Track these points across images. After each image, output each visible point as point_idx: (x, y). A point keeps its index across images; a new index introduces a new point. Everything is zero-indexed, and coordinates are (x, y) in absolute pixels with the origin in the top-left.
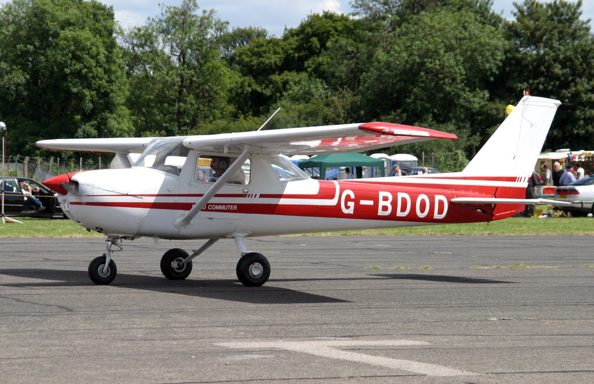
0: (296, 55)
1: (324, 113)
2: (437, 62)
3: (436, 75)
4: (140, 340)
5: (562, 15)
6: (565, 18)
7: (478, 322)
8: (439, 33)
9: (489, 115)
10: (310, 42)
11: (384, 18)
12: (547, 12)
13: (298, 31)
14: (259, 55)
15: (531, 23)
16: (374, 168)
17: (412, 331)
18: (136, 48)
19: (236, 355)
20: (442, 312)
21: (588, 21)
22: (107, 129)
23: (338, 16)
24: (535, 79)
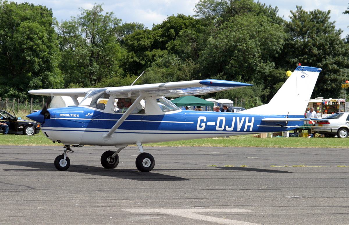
0: (161, 40)
1: (177, 74)
2: (245, 45)
3: (244, 53)
4: (77, 207)
5: (319, 18)
6: (320, 20)
7: (279, 199)
8: (246, 28)
9: (275, 77)
10: (169, 32)
11: (213, 19)
12: (310, 16)
13: (161, 25)
14: (138, 40)
15: (300, 23)
16: (207, 107)
17: (240, 204)
18: (65, 34)
19: (136, 216)
20: (257, 192)
21: (334, 23)
22: (48, 81)
23: (186, 17)
24: (302, 57)
